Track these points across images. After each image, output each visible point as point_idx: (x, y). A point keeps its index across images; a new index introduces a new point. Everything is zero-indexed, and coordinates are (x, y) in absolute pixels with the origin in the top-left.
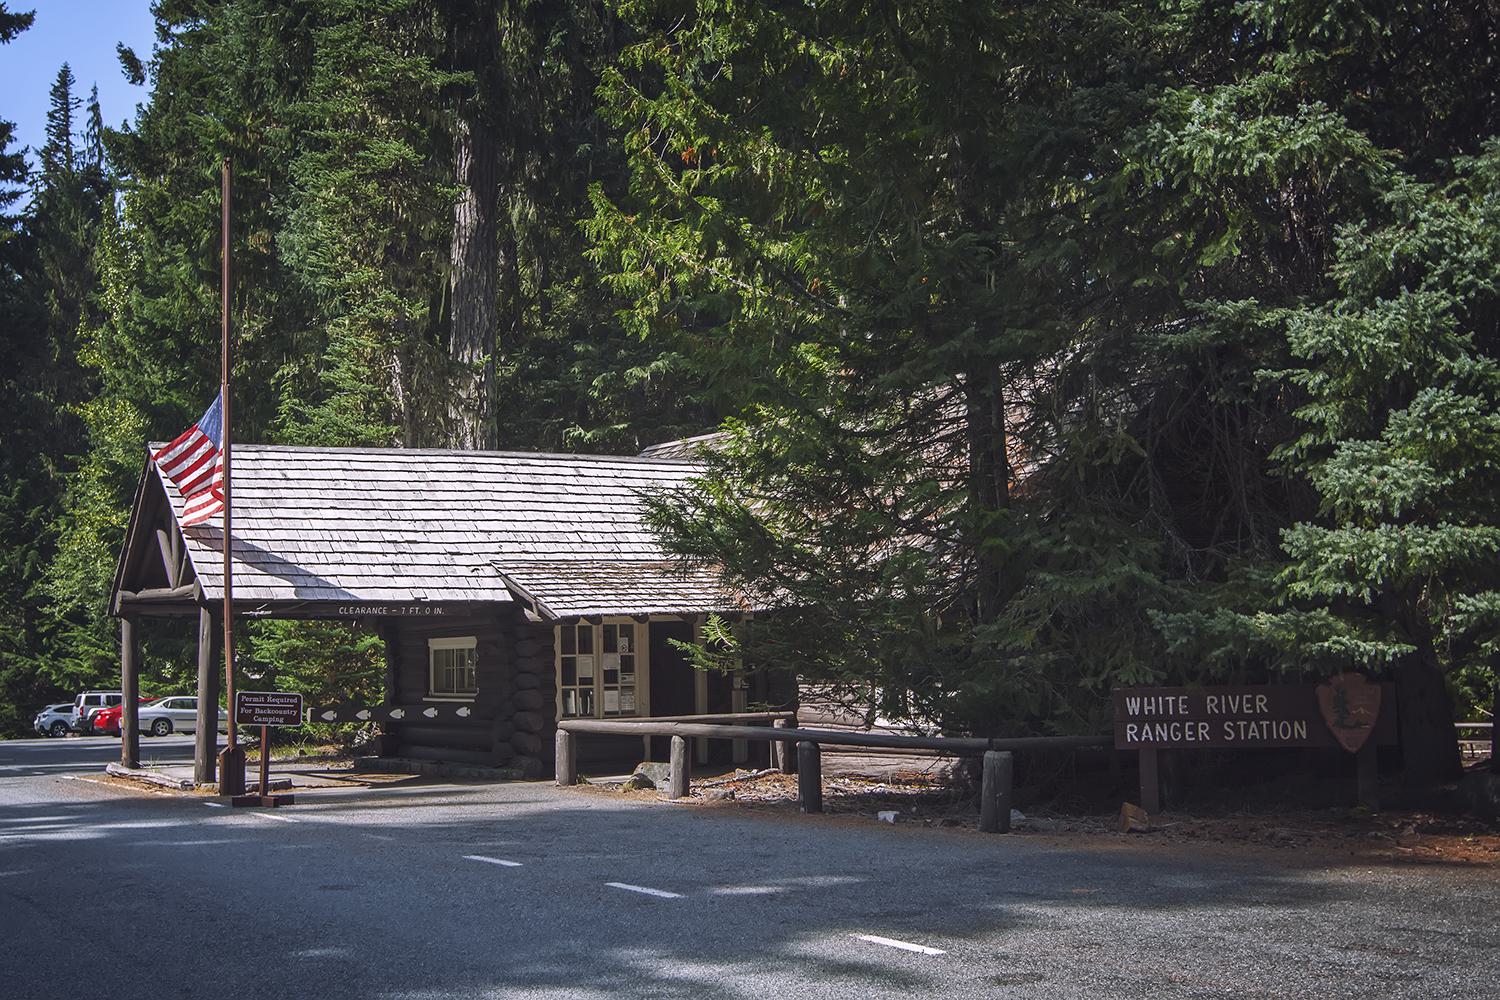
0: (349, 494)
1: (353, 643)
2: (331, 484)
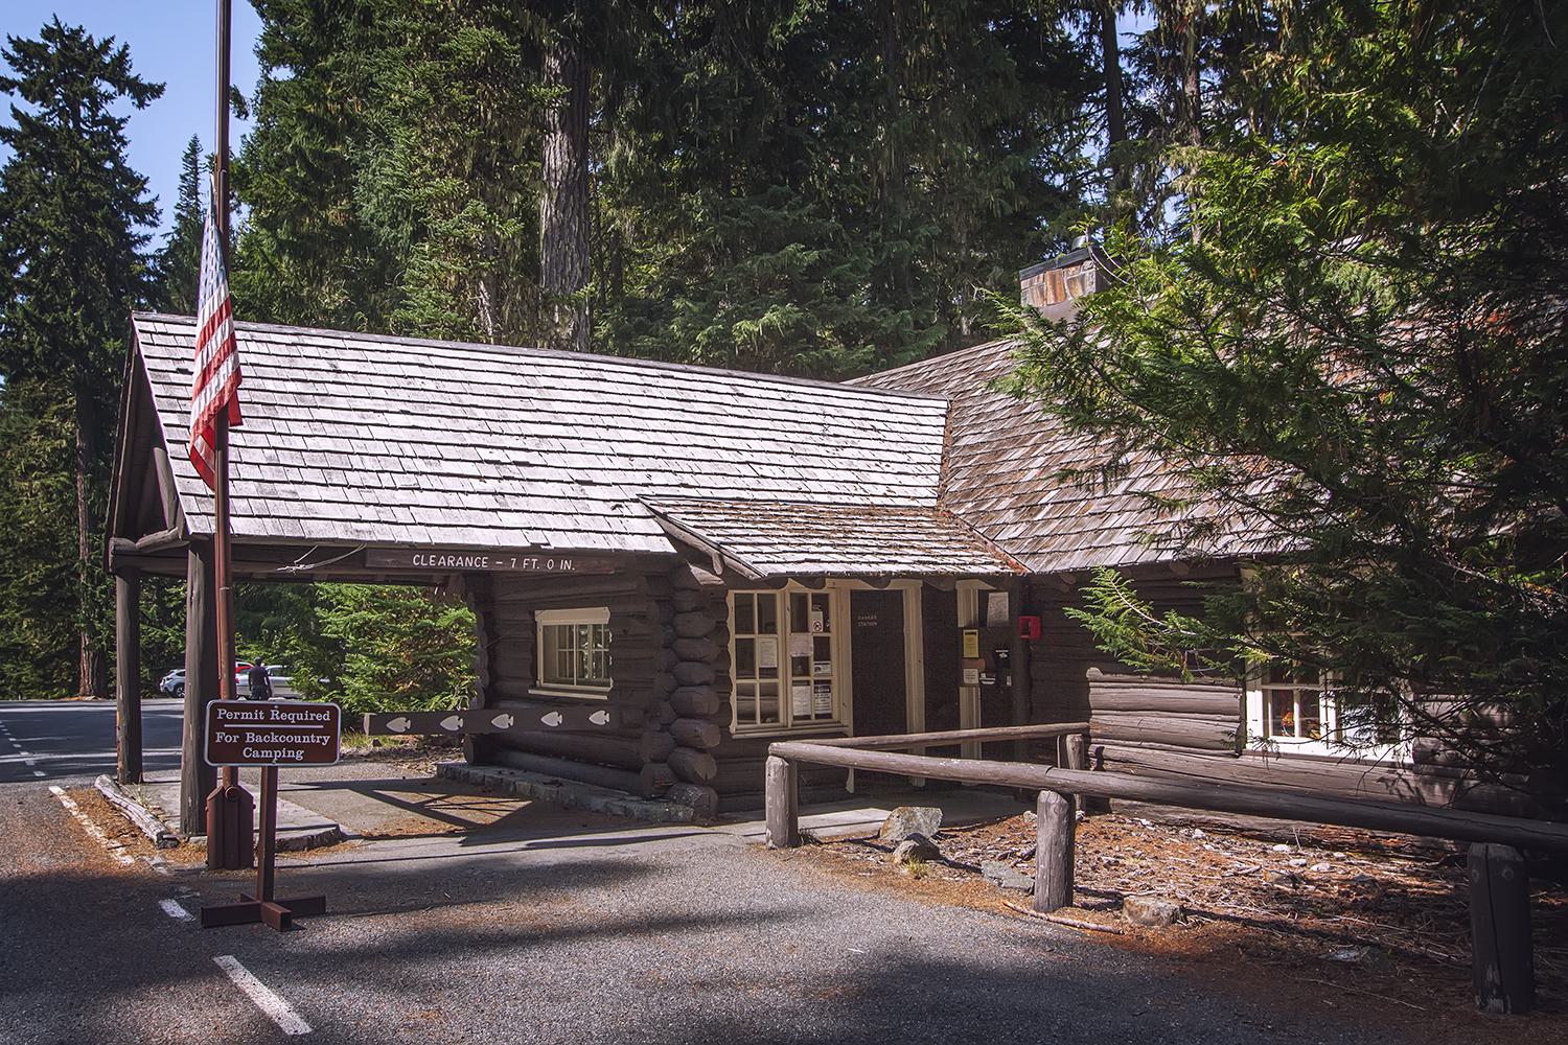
0: (429, 397)
1: (435, 616)
2: (403, 382)
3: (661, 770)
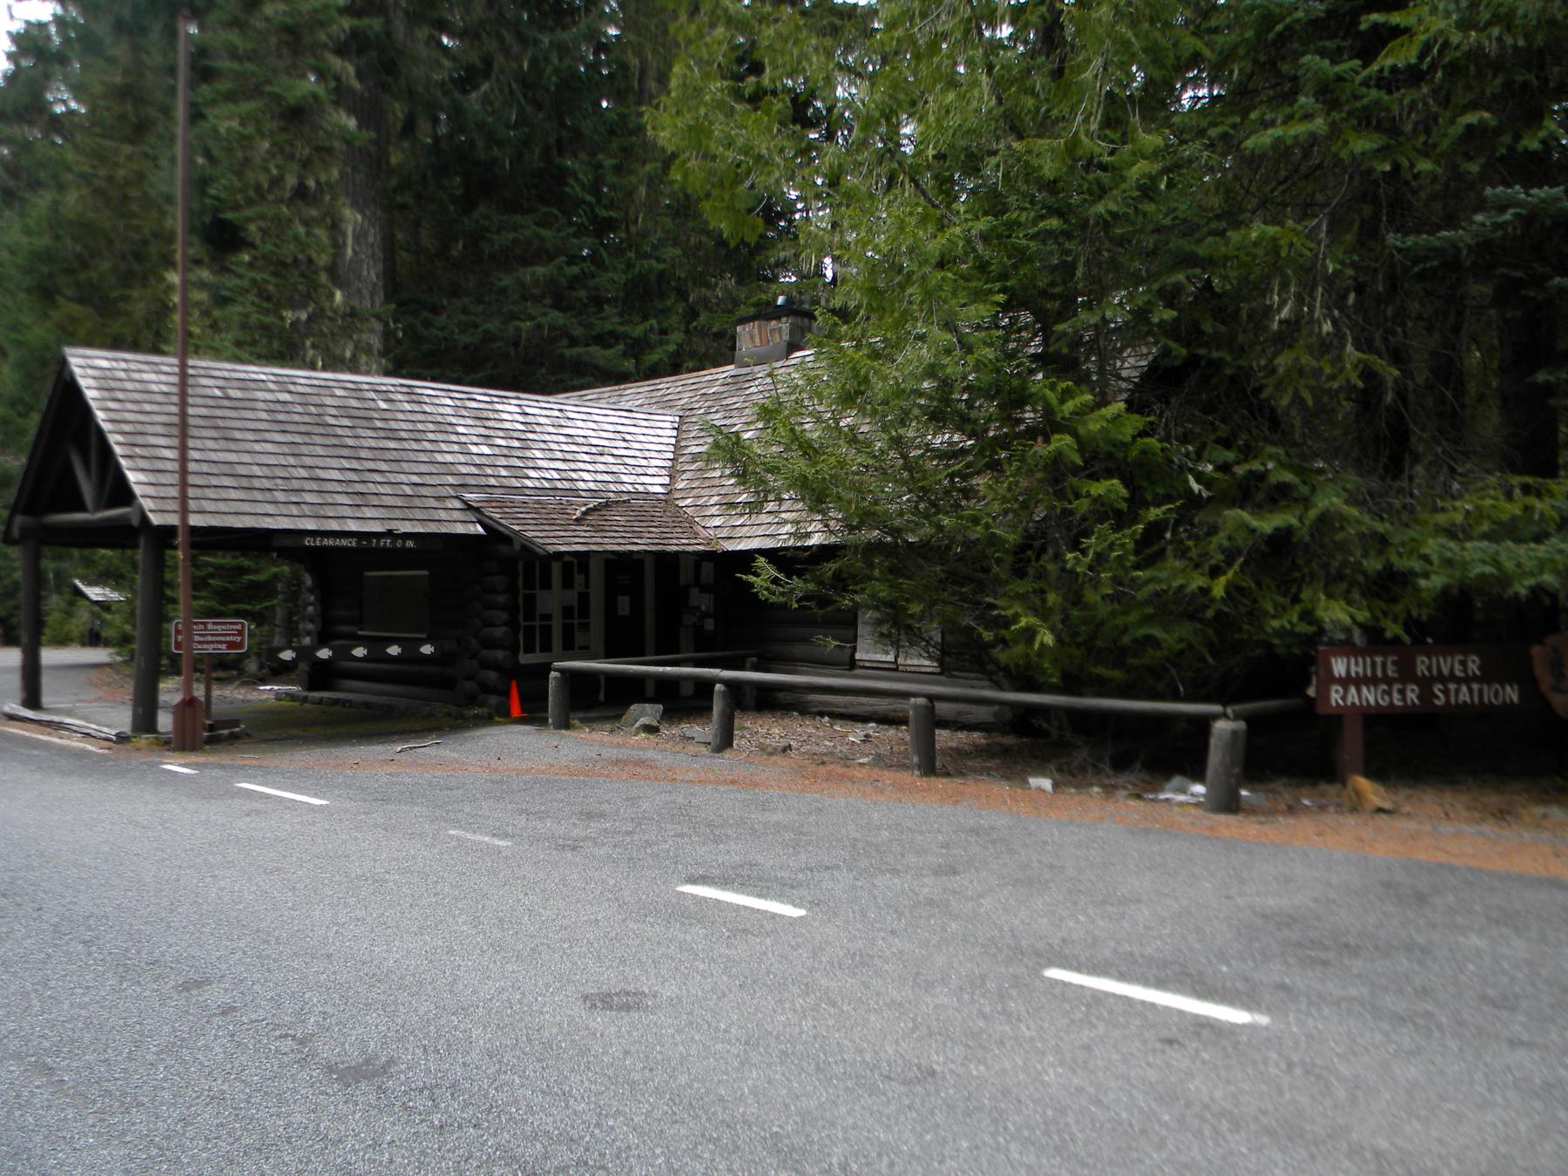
3: (470, 686)
